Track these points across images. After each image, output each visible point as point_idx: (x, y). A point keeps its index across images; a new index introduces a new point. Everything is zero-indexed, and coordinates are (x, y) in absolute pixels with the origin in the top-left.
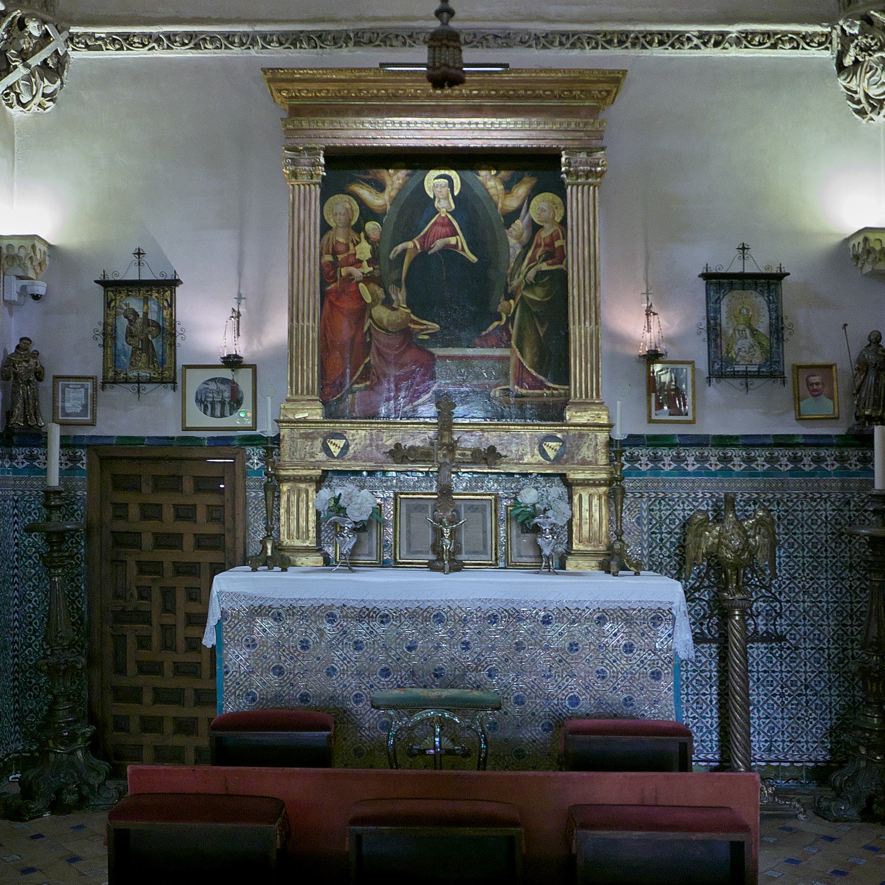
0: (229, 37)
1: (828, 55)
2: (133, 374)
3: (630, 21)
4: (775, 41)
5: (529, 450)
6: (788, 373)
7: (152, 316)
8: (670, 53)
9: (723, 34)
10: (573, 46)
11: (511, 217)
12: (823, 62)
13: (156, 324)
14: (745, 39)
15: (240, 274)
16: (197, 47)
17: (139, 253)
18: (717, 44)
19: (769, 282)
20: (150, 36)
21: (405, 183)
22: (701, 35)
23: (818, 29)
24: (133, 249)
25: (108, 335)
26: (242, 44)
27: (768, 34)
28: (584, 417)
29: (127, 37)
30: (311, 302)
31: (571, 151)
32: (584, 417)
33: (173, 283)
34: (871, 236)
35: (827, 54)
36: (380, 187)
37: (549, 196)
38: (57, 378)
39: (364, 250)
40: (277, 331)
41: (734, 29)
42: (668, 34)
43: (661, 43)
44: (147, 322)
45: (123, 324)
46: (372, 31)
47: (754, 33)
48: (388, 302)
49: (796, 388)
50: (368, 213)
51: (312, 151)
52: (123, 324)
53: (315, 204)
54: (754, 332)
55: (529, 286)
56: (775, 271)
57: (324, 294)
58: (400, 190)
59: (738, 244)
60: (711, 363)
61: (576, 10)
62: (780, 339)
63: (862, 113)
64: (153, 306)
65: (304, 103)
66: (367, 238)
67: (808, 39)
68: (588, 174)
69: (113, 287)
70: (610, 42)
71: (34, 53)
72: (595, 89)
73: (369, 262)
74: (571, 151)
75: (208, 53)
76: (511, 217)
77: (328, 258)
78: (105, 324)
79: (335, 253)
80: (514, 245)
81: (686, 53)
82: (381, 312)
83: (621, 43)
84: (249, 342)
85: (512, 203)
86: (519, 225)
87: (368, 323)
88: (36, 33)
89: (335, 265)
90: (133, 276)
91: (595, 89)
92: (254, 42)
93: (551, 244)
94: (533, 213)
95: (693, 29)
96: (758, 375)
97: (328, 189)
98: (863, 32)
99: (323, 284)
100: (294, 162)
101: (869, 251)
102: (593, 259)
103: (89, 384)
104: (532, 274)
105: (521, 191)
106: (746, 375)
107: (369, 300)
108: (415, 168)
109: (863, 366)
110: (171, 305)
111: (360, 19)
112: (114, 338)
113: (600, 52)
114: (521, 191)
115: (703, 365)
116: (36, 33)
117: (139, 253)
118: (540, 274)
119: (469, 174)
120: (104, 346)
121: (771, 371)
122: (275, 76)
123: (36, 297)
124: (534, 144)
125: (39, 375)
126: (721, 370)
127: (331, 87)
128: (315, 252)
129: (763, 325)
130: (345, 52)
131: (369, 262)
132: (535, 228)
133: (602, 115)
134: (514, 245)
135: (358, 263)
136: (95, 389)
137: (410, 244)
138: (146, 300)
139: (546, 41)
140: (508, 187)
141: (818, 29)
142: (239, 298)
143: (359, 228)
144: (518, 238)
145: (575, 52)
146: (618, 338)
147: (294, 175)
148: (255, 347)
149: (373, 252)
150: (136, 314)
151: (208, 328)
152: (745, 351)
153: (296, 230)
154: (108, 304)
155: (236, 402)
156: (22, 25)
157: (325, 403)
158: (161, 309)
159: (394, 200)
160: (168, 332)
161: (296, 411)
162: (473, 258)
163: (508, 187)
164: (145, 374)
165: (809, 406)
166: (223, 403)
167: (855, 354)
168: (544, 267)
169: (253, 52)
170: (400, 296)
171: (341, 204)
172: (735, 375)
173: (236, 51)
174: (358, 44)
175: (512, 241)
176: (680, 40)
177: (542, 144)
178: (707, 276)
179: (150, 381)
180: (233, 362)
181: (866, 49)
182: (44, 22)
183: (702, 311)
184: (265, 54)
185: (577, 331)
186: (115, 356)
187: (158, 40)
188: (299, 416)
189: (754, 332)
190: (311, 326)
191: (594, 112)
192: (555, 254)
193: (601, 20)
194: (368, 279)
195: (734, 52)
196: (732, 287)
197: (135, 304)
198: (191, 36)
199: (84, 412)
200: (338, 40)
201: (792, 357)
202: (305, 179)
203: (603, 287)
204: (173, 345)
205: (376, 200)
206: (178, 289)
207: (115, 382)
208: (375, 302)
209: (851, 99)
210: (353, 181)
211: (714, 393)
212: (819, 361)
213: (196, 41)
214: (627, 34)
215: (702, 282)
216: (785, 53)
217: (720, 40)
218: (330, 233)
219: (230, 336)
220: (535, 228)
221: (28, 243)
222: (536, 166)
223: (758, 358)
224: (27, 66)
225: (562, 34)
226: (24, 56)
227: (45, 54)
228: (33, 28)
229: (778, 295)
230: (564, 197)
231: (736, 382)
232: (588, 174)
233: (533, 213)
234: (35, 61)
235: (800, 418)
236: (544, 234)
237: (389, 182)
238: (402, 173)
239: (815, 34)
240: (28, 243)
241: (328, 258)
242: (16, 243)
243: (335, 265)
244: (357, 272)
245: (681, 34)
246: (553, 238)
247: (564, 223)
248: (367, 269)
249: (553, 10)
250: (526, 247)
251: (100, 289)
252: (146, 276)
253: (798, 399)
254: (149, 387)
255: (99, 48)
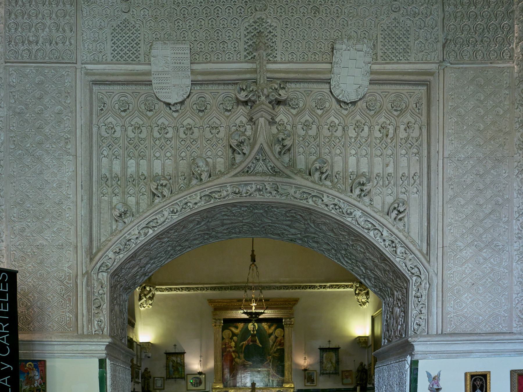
0: (197, 288)
1: (352, 290)
2: (174, 376)
3: (302, 282)
4: (339, 287)
5: (514, 296)
6: (340, 373)
7: (179, 362)
8: (312, 290)
9: (325, 286)
10: (287, 289)
11: (270, 335)
12: (351, 292)
13: (179, 363)
14: (331, 287)
15: (201, 350)
16: (189, 291)
17: (175, 345)
18: (324, 288)
19: (336, 350)
20: (177, 288)
21: (243, 327)
22: (320, 286)
23: (350, 284)
24: (174, 344)
25: (167, 366)
26: (201, 290)
27: (337, 285)
28: (288, 386)
29: (170, 288)
30: (219, 358)
31: (285, 319)
32: (288, 386)
33: (184, 353)
34: (361, 338)
35: (352, 290)
36: (237, 328)
37: (280, 329)
38: (154, 378)
39: (233, 344)
40: (211, 364)
41: (328, 284)
42: (311, 286)
43: (310, 288)
44: (177, 363)
45: (171, 363)
46: (235, 286)
47: (333, 285)
48: (239, 357)
49: (342, 376)
50: (234, 334)
51: (220, 320)
52: (171, 363)
53: (220, 333)
54: (332, 363)
55: (275, 353)
56: (337, 347)
57: (222, 355)
58: (242, 329)
59: (328, 340)
60: (321, 371)
61: (288, 279)
62: (338, 364)
63: (361, 305)
64: (179, 359)
65: (218, 307)
66: (234, 341)
67: (347, 286)
68: (290, 324)
69: (169, 354)
70: (296, 288)
71: (148, 294)
72: (292, 303)
73: (235, 347)
74: (285, 319)
75: (192, 292)
76: (270, 335)
77: (224, 346)
78: (167, 364)
79: (225, 345)
80: (271, 342)
81: (316, 290)
82: (237, 360)
83: (299, 288)
84: (204, 368)
85: (271, 331)
86: (272, 337)
87: (234, 362)
88: (148, 290)
89: (226, 348)
90: (173, 351)
91: (292, 303)
92: (204, 290)
93: (280, 342)
94: (276, 334)
95: (318, 284)
96: (333, 373)
97: (224, 328)
98: (360, 286)
99: (223, 353)
100: (215, 323)
101: (360, 342)
102: (291, 346)
103: (162, 379)
104: (275, 349)
105: (273, 328)
106: (329, 373)
107: (234, 357)
108: (246, 323)
109: (358, 371)
110: (184, 359)
111: (231, 283)
112: (169, 367)
113: (294, 290)
114: (273, 328)
115: (319, 371)
116: (148, 290)
117: (175, 345)
118: (277, 350)
119: (259, 324)
120: (166, 369)
121: (336, 373)
122: (211, 301)
123: (149, 357)
124: (276, 317)
125: (150, 377)
126: (323, 373)
127: (225, 304)
128: (220, 345)
129: (334, 361)
130: (227, 292)
131: (235, 347)
132: (276, 338)
133: (294, 308)
134: (271, 342)
135: (231, 347)
136: (164, 380)
137: (245, 342)
138: (177, 357)
139: (280, 288)
140: (270, 327)
141: (350, 284)
142: (201, 356)
143: (231, 338)
144: (272, 340)
145: (287, 291)
146: (297, 365)
147: (215, 326)
148: (205, 369)
149: (236, 344)
150: (174, 361)
151: (194, 364)
152: (329, 367)
153: (216, 340)
154: (167, 358)
155: (200, 383)
156: (145, 288)
157: (223, 383)
158: (181, 360)
159: (240, 331)
160: (182, 365)
161: (216, 385)
162: (261, 346)
163: (270, 327)
164: (177, 376)
165: (345, 381)
166: (197, 383)
167: (356, 368)
168: (279, 347)
169: (204, 292)
170: (242, 356)
171: (227, 332)
172: (327, 374)
173: (199, 292)
174: (231, 289)
175: (271, 341)
176: (314, 287)
177: (278, 317)
178: (320, 349)
179: (178, 378)
180: (200, 373)
181: (361, 290)
182: (150, 286)
183: (318, 358)
184: (206, 292)
185: (287, 364)
186: (169, 372)
187: (179, 289)
188: (217, 387)
189: (332, 363)
190: (220, 364)
191: (291, 308)
192: (282, 344)
193: (294, 283)
194: (234, 352)
195: (328, 290)
196: (326, 351)
197: (174, 358)
198: (187, 288)
199: (161, 386)
200: (226, 288)
201: (342, 368)
202: (218, 327)
203: (293, 352)
204: (184, 369)
205: (236, 331)
206: (185, 354)
207: (169, 378)
208: (235, 358)
209: (358, 301)
210: (230, 326)
211: (321, 378)
212: (348, 369)
213: (188, 289)
214: (301, 286)
215: (319, 350)
216: (342, 290)
217: (325, 287)
218: (224, 340)
219: (199, 366)
220: (276, 338)
221: (147, 344)
222: (276, 322)
223: (333, 369)
224: (146, 298)
225: (284, 286)
226: (145, 295)
227: (150, 295)
228: (148, 289)
229: (338, 353)
230: (283, 329)
231: (327, 375)
232: (290, 324)
233: (276, 334)
234: (147, 297)
235: (343, 384)
236: (279, 339)
237: (239, 326)
238: (243, 324)
239: (349, 285)
240: (147, 344)
241: (224, 346)
242: (145, 344)
243: (226, 348)
244: (231, 350)
245: (315, 286)
246: (281, 340)
247: (284, 336)
248: (234, 349)
249: (281, 279)
250: (274, 343)
251: (165, 355)
252: (177, 351)
253: (343, 379)
254: (178, 380)
255: (163, 291)
